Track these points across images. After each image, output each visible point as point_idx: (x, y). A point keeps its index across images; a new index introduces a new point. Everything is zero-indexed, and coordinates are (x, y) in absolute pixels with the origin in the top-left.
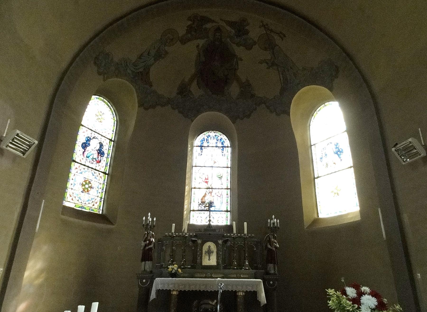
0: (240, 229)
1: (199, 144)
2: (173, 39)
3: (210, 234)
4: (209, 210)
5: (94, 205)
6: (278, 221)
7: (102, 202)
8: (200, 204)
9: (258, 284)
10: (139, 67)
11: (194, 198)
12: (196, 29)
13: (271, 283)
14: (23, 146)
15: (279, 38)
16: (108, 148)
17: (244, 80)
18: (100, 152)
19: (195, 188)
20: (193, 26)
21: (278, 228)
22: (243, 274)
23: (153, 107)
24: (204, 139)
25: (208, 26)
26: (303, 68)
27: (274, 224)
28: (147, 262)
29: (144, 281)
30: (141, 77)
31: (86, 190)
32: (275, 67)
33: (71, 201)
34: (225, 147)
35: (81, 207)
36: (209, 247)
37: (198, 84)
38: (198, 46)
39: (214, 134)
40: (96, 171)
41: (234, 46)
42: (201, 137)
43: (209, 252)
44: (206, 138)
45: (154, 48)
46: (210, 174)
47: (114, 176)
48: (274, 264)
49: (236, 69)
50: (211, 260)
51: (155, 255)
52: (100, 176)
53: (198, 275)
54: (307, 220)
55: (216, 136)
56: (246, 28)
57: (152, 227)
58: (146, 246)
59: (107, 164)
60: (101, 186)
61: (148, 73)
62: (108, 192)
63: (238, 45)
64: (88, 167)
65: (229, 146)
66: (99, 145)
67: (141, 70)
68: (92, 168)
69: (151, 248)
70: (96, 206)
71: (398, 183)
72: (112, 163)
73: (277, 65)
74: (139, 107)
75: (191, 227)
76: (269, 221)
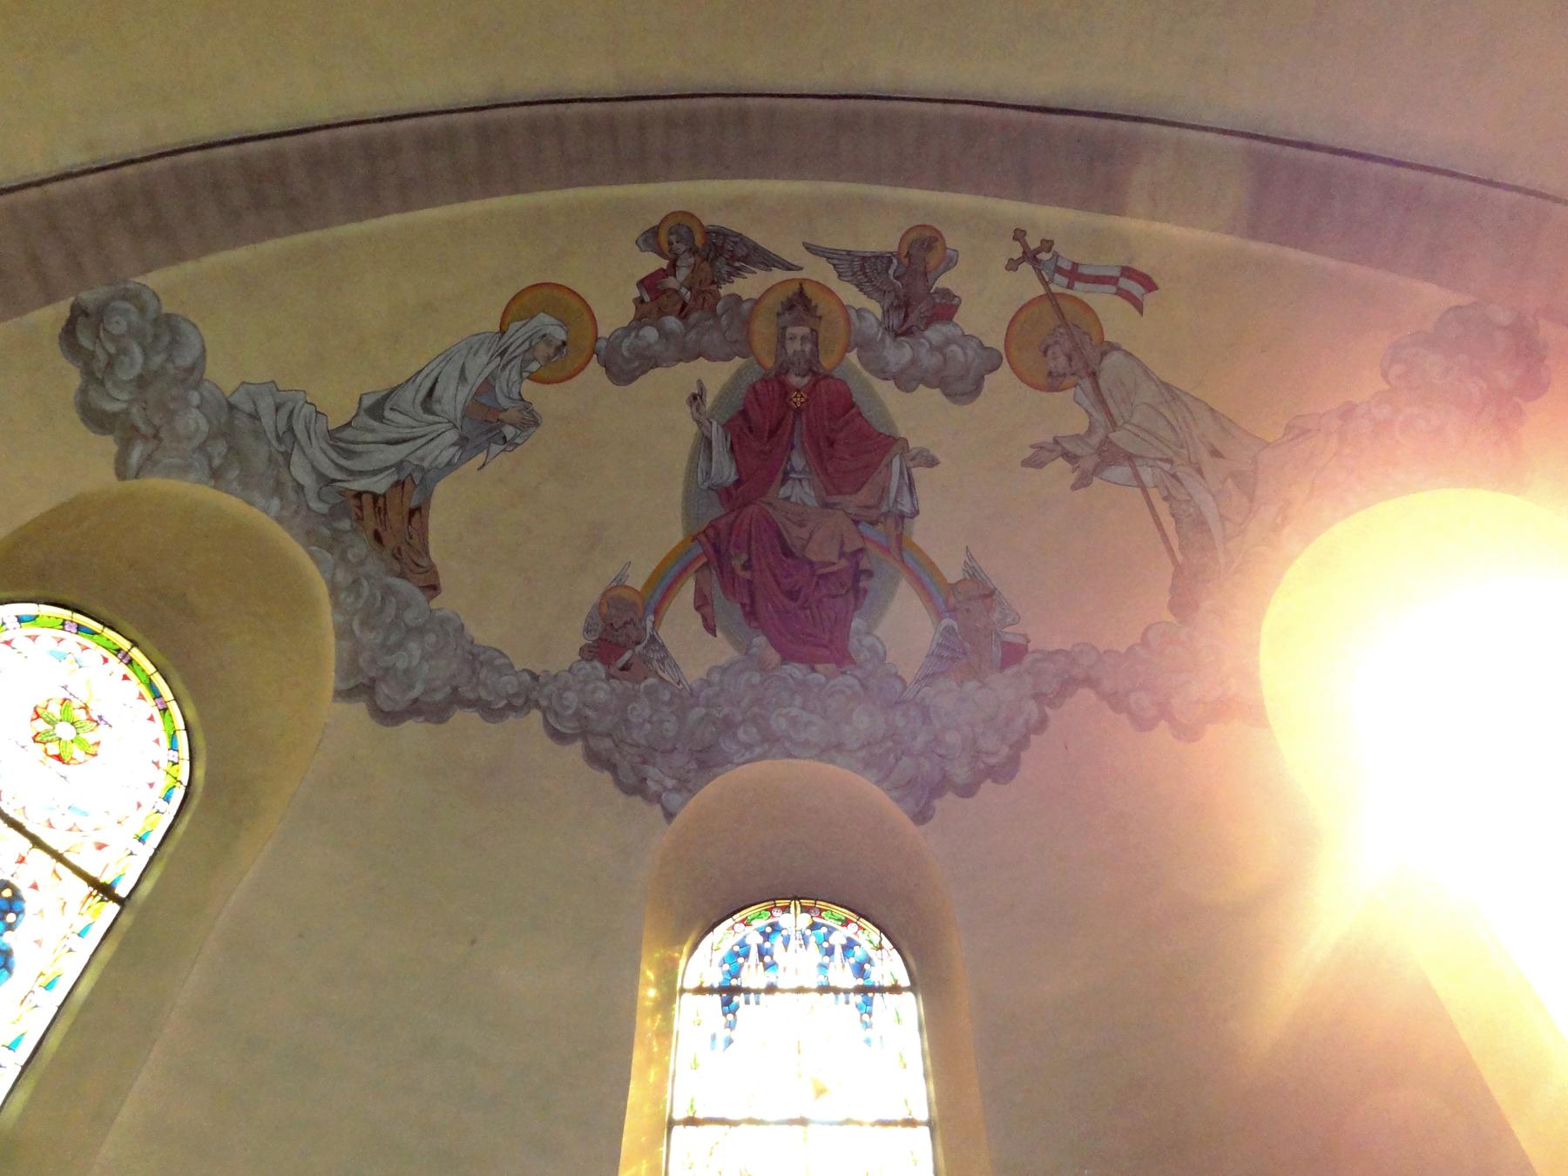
1: (716, 978)
2: (564, 343)
12: (684, 305)
15: (1120, 302)
17: (953, 574)
20: (671, 282)
23: (433, 711)
24: (742, 944)
25: (749, 285)
32: (1121, 472)
34: (881, 990)
38: (696, 399)
39: (805, 919)
41: (886, 391)
42: (724, 936)
44: (754, 939)
45: (463, 377)
49: (902, 516)
55: (814, 926)
63: (906, 380)
65: (905, 981)
67: (380, 484)
73: (1130, 457)
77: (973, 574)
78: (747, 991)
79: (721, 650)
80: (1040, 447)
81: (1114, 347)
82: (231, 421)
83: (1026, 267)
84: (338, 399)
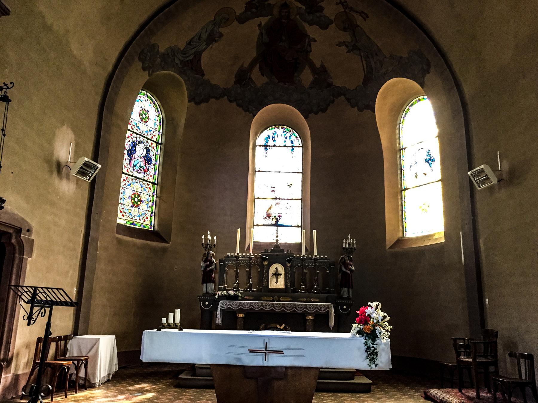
0: (309, 250)
1: (263, 143)
3: (277, 255)
4: (276, 225)
5: (144, 221)
6: (355, 241)
7: (153, 217)
8: (266, 218)
9: (328, 307)
10: (187, 55)
11: (258, 211)
13: (345, 307)
14: (87, 171)
16: (156, 155)
18: (147, 159)
19: (258, 198)
21: (355, 249)
22: (314, 298)
23: (206, 100)
26: (390, 56)
27: (349, 244)
28: (209, 284)
29: (207, 303)
30: (191, 65)
31: (136, 205)
33: (122, 217)
34: (296, 147)
35: (132, 224)
36: (277, 269)
37: (260, 69)
38: (260, 25)
40: (144, 182)
41: (306, 25)
43: (277, 275)
45: (206, 31)
46: (277, 178)
47: (165, 186)
48: (349, 288)
50: (279, 283)
51: (216, 277)
52: (149, 186)
53: (265, 298)
54: (390, 238)
56: (320, 4)
57: (213, 247)
58: (207, 266)
59: (155, 172)
60: (151, 199)
61: (200, 60)
62: (159, 206)
63: (311, 24)
64: (136, 177)
66: (145, 150)
67: (190, 58)
68: (140, 179)
69: (212, 270)
70: (147, 222)
71: (478, 205)
72: (160, 170)
73: (359, 50)
74: (189, 101)
75: (257, 246)
76: (344, 241)
77: (323, 66)
78: (270, 146)
79: (265, 79)
80: (340, 42)
81: (358, 26)
82: (164, 56)
83: (340, 5)
84: (182, 45)
